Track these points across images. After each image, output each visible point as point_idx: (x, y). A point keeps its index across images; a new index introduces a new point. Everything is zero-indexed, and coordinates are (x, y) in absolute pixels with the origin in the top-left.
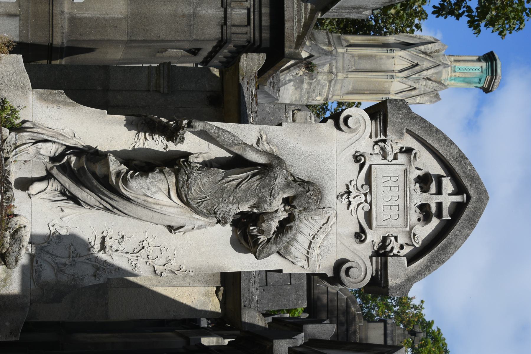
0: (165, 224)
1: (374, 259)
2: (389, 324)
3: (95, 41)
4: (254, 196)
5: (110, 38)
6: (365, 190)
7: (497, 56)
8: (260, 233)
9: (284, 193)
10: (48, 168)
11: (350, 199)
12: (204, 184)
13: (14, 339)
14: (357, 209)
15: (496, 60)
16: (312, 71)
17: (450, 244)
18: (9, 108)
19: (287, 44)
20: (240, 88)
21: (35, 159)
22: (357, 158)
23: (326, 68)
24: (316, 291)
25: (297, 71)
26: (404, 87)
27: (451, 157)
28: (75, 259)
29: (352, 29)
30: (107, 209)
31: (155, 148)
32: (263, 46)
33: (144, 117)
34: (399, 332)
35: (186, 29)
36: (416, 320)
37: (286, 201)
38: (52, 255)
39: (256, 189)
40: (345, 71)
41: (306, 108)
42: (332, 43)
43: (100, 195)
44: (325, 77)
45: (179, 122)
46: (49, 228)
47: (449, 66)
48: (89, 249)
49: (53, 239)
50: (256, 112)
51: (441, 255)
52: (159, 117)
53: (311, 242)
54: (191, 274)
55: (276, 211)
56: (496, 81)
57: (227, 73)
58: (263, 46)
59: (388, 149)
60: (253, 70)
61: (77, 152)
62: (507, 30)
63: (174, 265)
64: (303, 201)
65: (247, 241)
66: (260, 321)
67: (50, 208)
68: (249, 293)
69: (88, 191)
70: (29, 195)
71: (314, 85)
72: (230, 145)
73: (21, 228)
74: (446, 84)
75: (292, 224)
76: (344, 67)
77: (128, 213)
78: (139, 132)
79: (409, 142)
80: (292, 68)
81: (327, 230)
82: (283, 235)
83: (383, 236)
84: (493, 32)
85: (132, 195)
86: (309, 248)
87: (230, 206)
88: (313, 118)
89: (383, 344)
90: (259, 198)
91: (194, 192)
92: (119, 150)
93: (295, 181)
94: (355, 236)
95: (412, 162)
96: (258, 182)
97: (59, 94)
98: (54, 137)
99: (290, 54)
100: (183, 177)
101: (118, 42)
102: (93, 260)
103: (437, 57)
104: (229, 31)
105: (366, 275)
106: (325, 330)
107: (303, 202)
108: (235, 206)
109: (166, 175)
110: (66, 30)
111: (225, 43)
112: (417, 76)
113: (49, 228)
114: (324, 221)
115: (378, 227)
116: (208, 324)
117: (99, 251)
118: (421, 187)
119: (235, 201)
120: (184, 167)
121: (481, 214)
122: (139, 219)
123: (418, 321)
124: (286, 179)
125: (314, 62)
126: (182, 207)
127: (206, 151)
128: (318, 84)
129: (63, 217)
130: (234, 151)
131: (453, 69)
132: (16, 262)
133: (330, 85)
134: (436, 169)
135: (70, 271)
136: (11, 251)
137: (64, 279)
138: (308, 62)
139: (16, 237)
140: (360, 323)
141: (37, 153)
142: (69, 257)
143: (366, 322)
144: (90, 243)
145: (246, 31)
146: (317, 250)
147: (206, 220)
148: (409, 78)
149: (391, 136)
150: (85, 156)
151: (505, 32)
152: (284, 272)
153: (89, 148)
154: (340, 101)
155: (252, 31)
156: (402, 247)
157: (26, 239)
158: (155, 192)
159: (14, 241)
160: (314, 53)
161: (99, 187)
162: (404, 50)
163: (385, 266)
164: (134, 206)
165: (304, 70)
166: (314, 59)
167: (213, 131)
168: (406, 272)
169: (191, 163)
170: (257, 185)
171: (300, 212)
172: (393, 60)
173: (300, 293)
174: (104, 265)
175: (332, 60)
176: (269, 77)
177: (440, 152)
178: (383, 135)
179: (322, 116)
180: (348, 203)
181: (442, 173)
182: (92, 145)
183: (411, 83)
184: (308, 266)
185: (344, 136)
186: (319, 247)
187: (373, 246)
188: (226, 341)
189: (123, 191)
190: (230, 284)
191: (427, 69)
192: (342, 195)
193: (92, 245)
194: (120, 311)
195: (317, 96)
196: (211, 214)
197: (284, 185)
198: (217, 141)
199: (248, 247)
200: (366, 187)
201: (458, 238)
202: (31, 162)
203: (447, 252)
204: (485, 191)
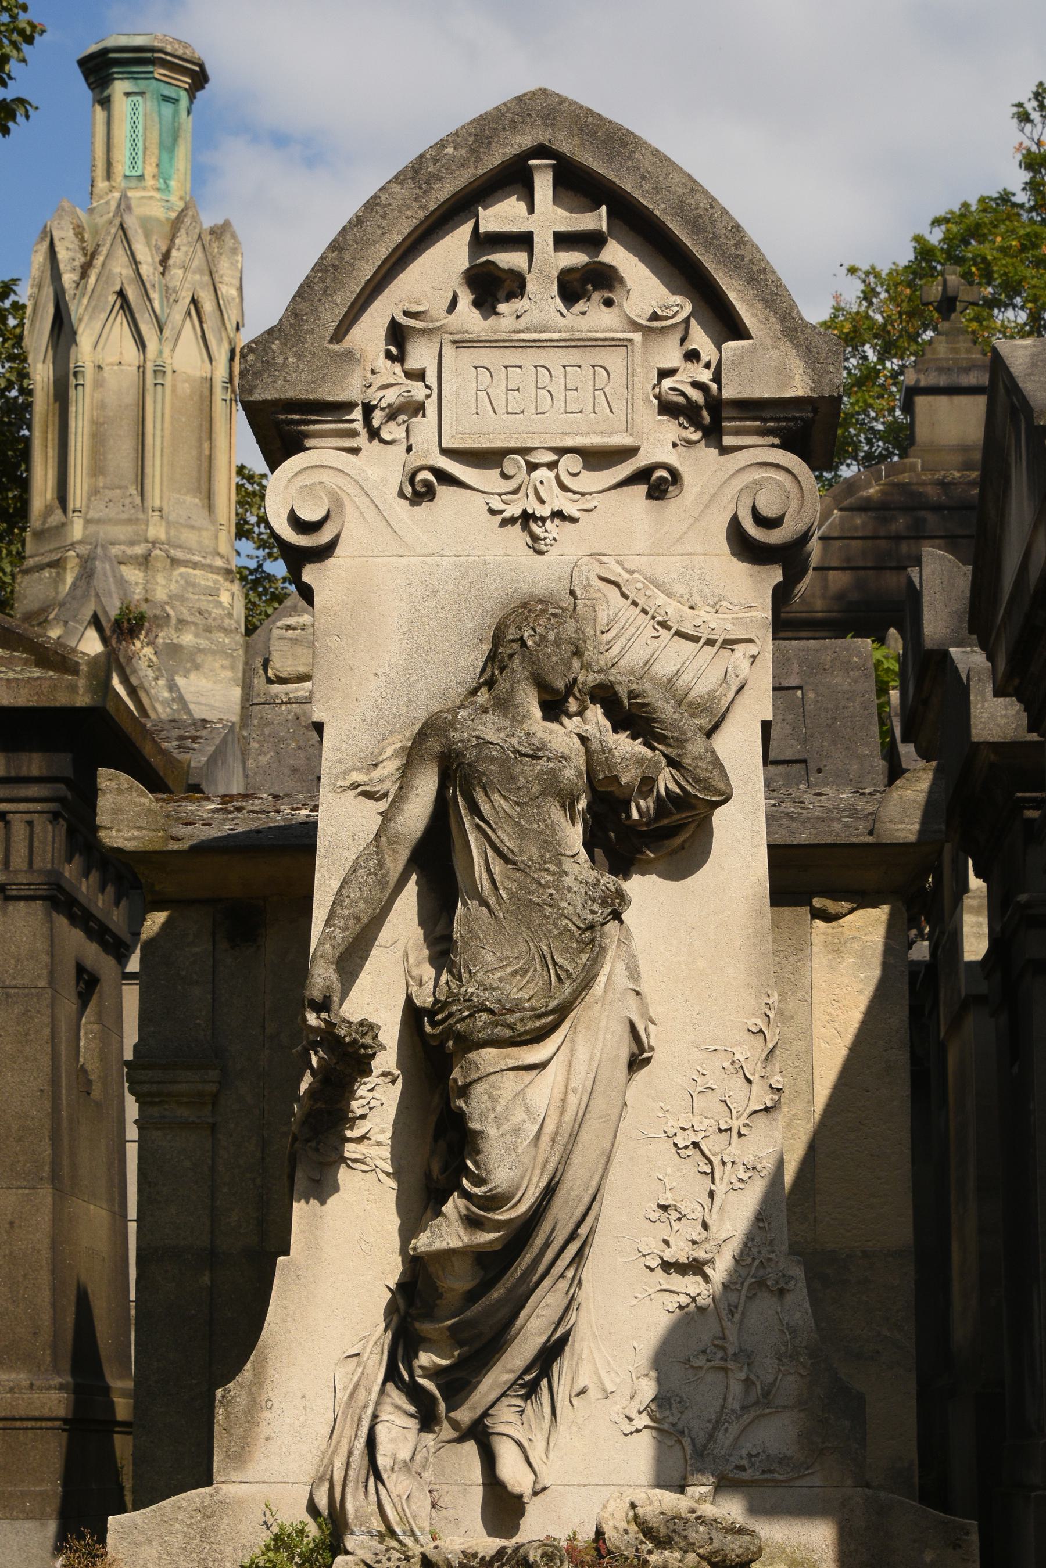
0: (625, 1081)
1: (728, 441)
2: (918, 381)
3: (54, 1290)
4: (539, 807)
5: (47, 1241)
6: (519, 467)
7: (93, 48)
8: (651, 791)
9: (527, 717)
10: (454, 1435)
11: (547, 513)
12: (501, 960)
13: (975, 1538)
14: (575, 493)
15: (105, 51)
16: (141, 618)
17: (681, 208)
18: (271, 1554)
19: (62, 700)
20: (201, 849)
21: (425, 1475)
22: (420, 492)
23: (133, 575)
24: (819, 604)
25: (143, 664)
26: (189, 335)
27: (416, 205)
28: (731, 1351)
29: (10, 495)
30: (579, 1257)
31: (390, 1111)
32: (69, 773)
33: (297, 1145)
34: (942, 349)
35: (18, 1009)
36: (908, 291)
37: (554, 708)
38: (717, 1424)
39: (517, 803)
40: (141, 516)
41: (255, 636)
42: (55, 557)
43: (535, 1278)
44: (160, 579)
45: (311, 1037)
46: (638, 1431)
47: (124, 197)
48: (701, 1309)
49: (671, 1419)
50: (276, 797)
51: (715, 237)
52: (298, 1099)
53: (679, 634)
54: (775, 998)
55: (584, 739)
56: (169, 49)
57: (157, 888)
58: (69, 773)
59: (391, 396)
60: (150, 810)
61: (405, 1348)
62: (14, 17)
63: (749, 1051)
64: (552, 657)
65: (674, 831)
66: (917, 787)
67: (574, 1429)
68: (832, 820)
69: (523, 1314)
70: (535, 1493)
71: (185, 611)
72: (382, 883)
73: (636, 1516)
74: (181, 205)
75: (622, 692)
76: (129, 521)
77: (591, 1191)
78: (344, 1160)
79: (369, 334)
80: (134, 681)
81: (639, 585)
82: (654, 720)
83: (660, 414)
84: (24, 61)
85: (535, 1180)
86: (695, 639)
87: (568, 881)
88: (292, 621)
89: (982, 400)
90: (544, 793)
91: (526, 991)
92: (398, 1222)
93: (490, 684)
94: (657, 499)
95: (431, 325)
96: (496, 797)
97: (227, 1404)
98: (360, 1419)
99: (92, 690)
100: (480, 1024)
101: (57, 1219)
102: (733, 1298)
103: (96, 232)
104: (22, 878)
105: (778, 466)
106: (941, 580)
107: (554, 659)
108: (568, 865)
109: (474, 1076)
110: (22, 1377)
111: (60, 888)
112: (155, 296)
113: (638, 1431)
114: (613, 592)
115: (630, 428)
116: (921, 936)
117: (706, 1278)
118: (509, 297)
119: (553, 868)
120: (451, 1021)
121: (589, 112)
122: (609, 1157)
123: (910, 284)
124: (486, 711)
125: (114, 613)
126: (573, 1028)
127: (400, 954)
128: (181, 598)
129: (604, 1390)
130: (400, 868)
131: (133, 184)
132: (741, 1531)
133: (186, 563)
134: (452, 252)
135: (767, 1369)
136: (709, 1548)
137: (791, 1385)
138: (114, 631)
139: (663, 1531)
140: (916, 469)
141: (409, 1470)
142: (725, 1370)
143: (912, 450)
144: (681, 1307)
145: (23, 826)
146: (703, 614)
147: (610, 954)
148: (163, 320)
149: (351, 390)
150: (417, 1325)
151: (22, 24)
152: (769, 717)
153: (391, 1310)
154: (233, 530)
155: (23, 806)
156: (692, 356)
157: (669, 1500)
158: (528, 1111)
159: (676, 1539)
160: (87, 614)
161: (512, 1280)
162: (75, 333)
163: (750, 408)
164: (569, 1174)
165: (138, 644)
166: (106, 612)
167: (339, 935)
168: (769, 342)
169: (436, 1001)
170: (506, 798)
171: (586, 667)
172: (106, 368)
173: (827, 658)
174: (749, 1265)
175: (106, 557)
176: (165, 753)
177: (400, 238)
178: (350, 412)
179: (280, 585)
180: (557, 521)
181: (467, 229)
182: (384, 1303)
183: (177, 314)
184: (751, 641)
185: (355, 535)
186: (692, 608)
187: (690, 443)
188: (975, 883)
189: (523, 1208)
190: (804, 878)
191: (135, 263)
192: (535, 538)
193: (688, 1300)
194: (883, 1215)
195: (219, 604)
196: (593, 940)
197: (505, 715)
198: (371, 921)
199: (693, 826)
200: (510, 464)
201: (663, 183)
202: (434, 1487)
203: (709, 217)
204: (519, 99)
